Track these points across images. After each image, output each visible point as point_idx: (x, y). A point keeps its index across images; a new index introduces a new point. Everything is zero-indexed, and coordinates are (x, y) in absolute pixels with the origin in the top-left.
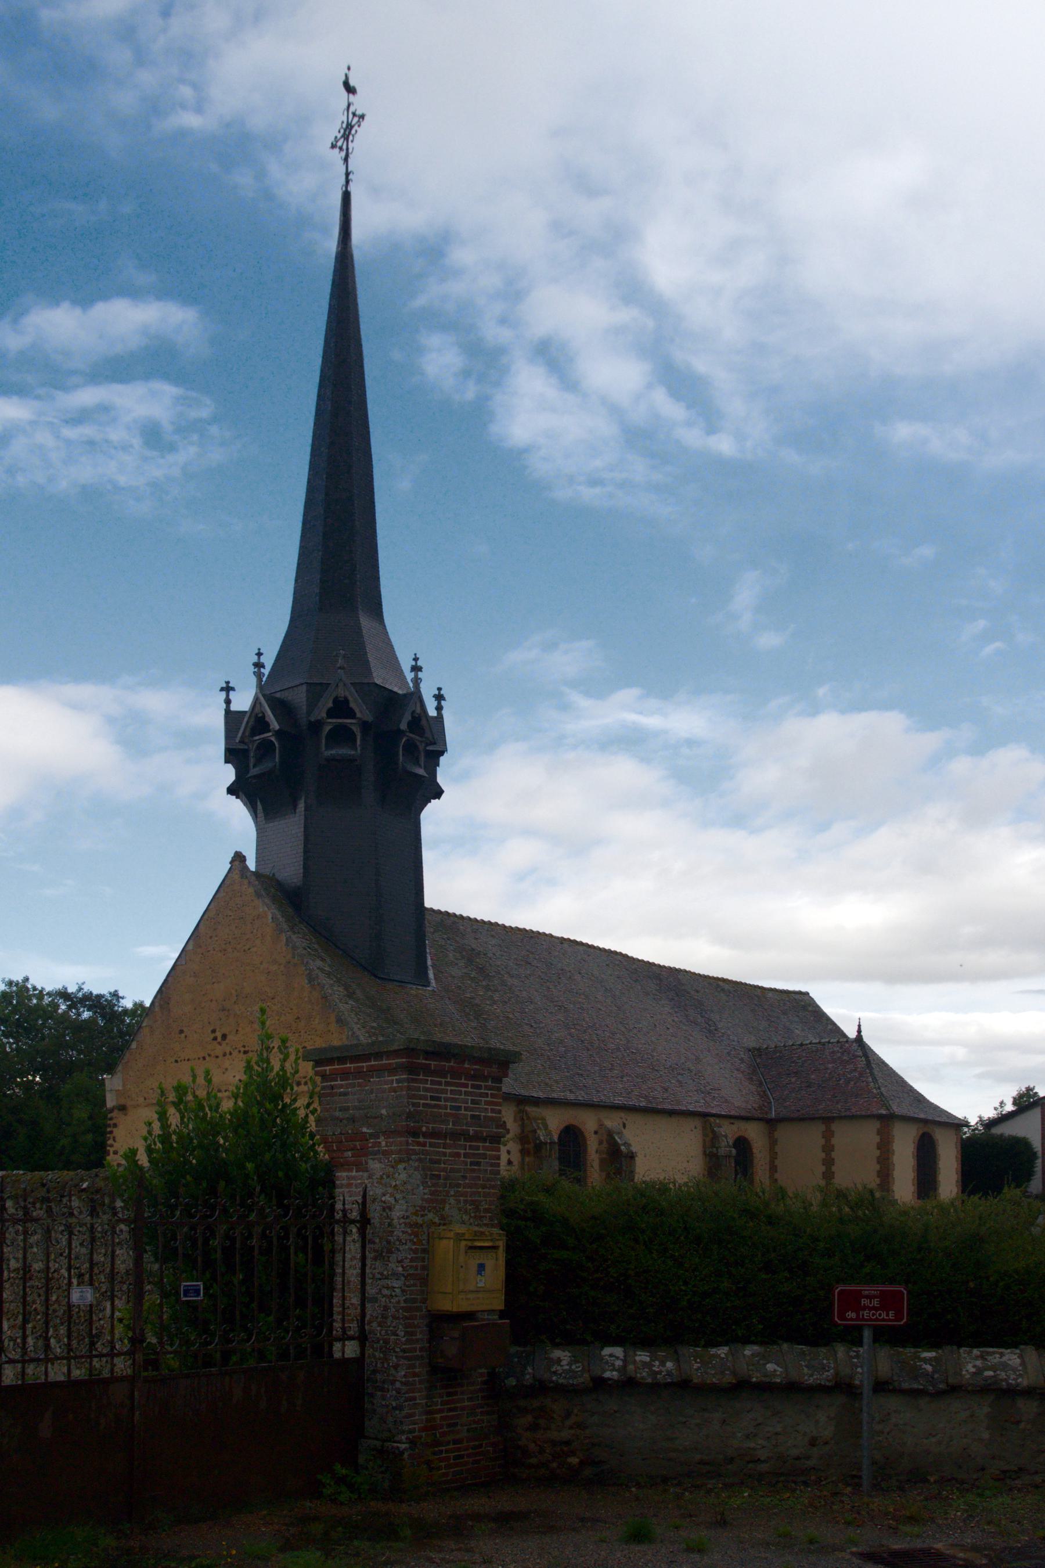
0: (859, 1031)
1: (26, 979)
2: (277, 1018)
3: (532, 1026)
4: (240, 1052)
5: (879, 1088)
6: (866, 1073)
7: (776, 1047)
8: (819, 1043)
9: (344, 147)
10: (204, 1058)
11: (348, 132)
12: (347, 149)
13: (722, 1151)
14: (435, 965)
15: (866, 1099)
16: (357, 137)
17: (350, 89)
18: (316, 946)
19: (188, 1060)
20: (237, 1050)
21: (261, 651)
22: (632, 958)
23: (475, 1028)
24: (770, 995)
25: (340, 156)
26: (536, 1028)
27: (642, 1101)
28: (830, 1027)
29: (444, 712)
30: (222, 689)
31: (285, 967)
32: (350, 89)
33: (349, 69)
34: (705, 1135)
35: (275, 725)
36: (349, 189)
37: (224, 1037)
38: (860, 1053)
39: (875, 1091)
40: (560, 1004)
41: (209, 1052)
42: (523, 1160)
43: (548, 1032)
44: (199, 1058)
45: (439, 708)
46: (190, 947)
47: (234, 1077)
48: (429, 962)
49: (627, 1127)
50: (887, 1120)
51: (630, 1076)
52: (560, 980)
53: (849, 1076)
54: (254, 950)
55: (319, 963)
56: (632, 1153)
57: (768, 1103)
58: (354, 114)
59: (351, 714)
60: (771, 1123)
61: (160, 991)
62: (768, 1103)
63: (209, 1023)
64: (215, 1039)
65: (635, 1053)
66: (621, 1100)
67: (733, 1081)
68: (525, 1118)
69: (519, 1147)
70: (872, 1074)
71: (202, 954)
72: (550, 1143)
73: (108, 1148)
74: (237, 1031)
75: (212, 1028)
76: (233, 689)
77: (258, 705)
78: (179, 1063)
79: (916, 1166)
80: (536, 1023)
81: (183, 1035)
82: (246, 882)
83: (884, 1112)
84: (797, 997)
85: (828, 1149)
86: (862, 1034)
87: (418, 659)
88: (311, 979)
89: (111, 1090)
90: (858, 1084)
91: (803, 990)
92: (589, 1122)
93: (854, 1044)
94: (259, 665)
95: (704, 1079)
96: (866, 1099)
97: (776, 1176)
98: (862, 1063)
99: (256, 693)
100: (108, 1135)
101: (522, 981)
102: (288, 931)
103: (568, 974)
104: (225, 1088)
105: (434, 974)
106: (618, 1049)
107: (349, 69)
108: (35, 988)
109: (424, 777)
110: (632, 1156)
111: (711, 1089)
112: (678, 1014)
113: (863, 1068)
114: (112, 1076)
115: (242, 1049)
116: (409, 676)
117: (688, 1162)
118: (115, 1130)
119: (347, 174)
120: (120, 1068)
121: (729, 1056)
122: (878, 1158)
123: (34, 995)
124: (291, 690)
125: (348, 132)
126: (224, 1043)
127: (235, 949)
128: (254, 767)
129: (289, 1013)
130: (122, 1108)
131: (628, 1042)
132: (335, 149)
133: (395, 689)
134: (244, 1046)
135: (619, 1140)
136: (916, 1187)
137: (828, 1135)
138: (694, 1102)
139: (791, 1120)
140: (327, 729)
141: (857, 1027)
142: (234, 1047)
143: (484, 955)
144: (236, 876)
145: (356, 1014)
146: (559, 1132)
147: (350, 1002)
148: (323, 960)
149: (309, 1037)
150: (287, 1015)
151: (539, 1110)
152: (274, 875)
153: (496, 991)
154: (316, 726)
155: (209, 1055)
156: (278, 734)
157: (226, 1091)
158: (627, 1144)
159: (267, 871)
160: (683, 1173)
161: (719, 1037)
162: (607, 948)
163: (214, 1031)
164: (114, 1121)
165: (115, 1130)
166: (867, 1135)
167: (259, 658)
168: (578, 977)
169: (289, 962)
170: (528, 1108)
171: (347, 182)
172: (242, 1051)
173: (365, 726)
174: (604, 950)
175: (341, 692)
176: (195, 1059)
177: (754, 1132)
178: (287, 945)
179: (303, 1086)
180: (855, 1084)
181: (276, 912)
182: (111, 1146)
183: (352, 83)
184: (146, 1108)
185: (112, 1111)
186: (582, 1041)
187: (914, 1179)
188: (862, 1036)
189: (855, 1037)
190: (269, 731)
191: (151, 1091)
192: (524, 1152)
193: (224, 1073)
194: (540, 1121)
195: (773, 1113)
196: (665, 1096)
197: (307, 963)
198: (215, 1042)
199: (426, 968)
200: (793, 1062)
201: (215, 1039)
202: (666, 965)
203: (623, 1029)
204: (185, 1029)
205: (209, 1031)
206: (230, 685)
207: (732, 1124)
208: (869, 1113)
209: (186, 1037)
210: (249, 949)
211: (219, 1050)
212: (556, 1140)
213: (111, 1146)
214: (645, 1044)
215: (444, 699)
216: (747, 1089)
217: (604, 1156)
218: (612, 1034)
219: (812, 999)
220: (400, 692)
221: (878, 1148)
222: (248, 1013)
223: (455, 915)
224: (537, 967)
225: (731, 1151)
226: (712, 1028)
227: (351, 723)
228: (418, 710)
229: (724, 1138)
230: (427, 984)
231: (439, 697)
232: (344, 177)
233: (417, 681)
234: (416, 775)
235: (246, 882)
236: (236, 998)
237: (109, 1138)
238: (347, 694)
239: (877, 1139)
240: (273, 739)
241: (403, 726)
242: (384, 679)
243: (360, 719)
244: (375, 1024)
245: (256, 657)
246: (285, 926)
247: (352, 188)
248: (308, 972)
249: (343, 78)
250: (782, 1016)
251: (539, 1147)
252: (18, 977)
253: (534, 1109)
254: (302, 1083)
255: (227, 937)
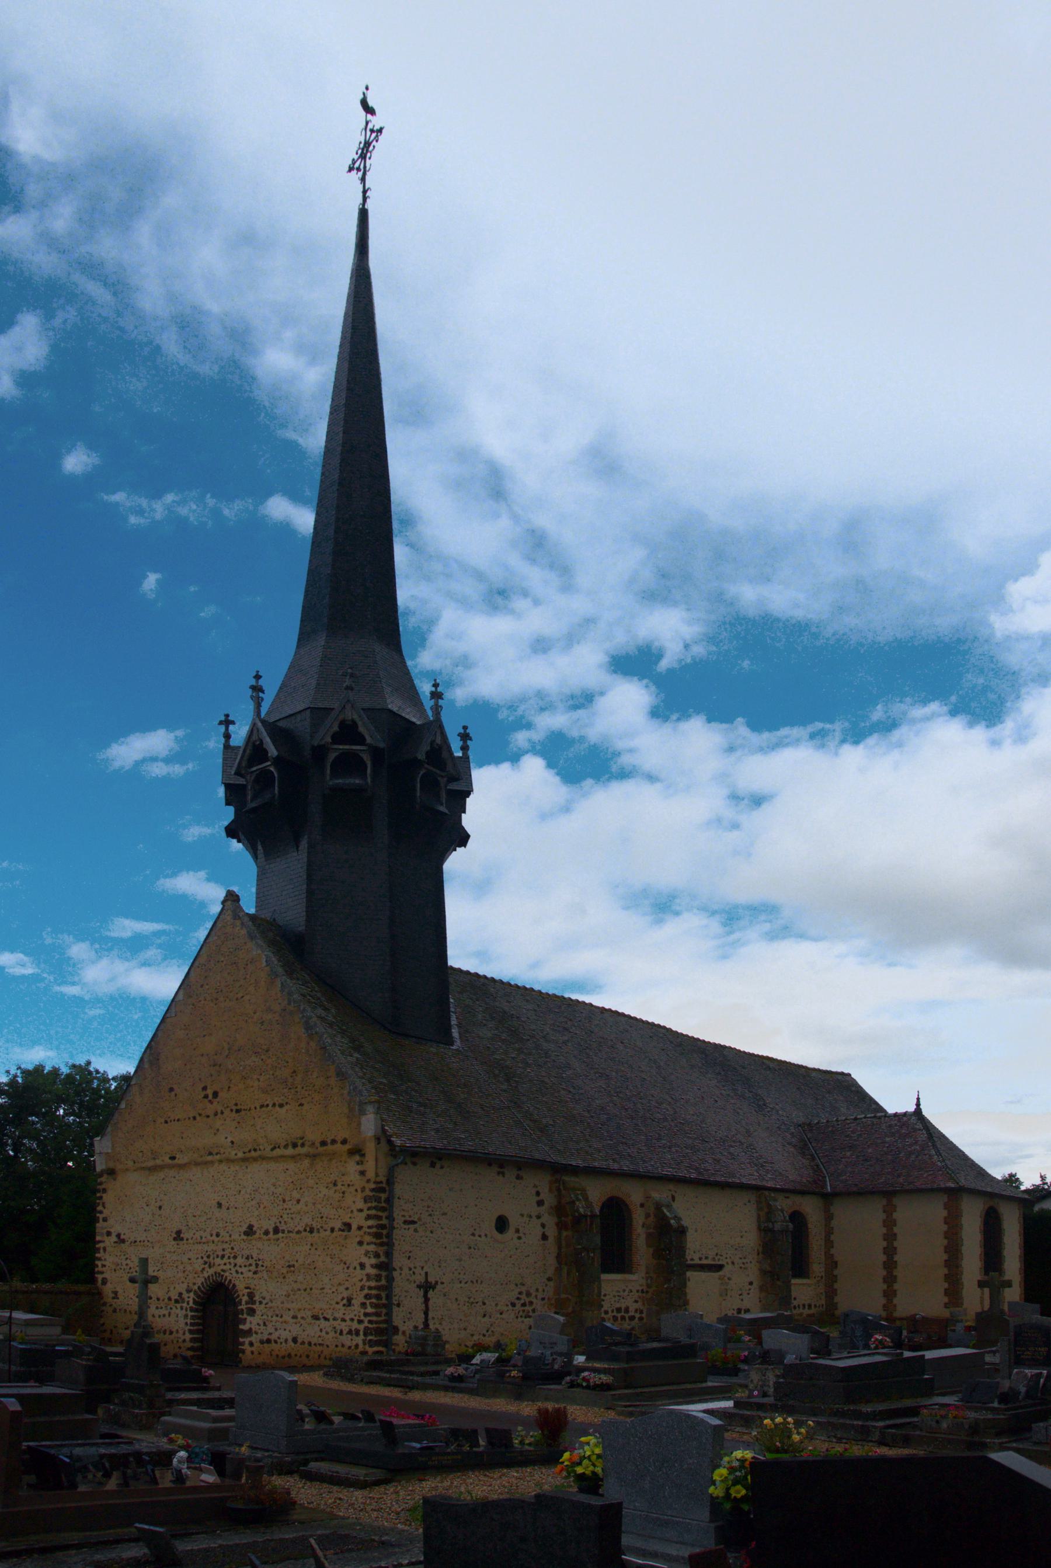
0: (918, 1104)
1: (89, 1063)
2: (271, 1073)
3: (570, 1092)
4: (232, 1110)
5: (944, 1161)
6: (928, 1146)
7: (828, 1121)
8: (875, 1117)
9: (362, 167)
10: (194, 1118)
11: (365, 150)
12: (365, 167)
13: (778, 1226)
14: (460, 1024)
15: (932, 1172)
16: (374, 152)
17: (369, 110)
18: (319, 995)
19: (178, 1120)
20: (229, 1109)
21: (260, 674)
22: (676, 1032)
23: (505, 1091)
24: (814, 1074)
25: (357, 177)
26: (575, 1094)
27: (693, 1173)
28: (874, 1106)
29: (470, 753)
30: (221, 723)
31: (280, 1015)
32: (369, 110)
33: (367, 88)
34: (759, 1209)
35: (273, 751)
36: (366, 207)
37: (215, 1094)
38: (920, 1126)
39: (939, 1164)
40: (601, 1071)
41: (200, 1112)
42: (560, 1233)
43: (588, 1098)
44: (189, 1118)
45: (465, 748)
46: (181, 997)
47: (226, 1138)
48: (454, 1021)
49: (677, 1199)
50: (954, 1194)
51: (678, 1146)
52: (601, 1048)
53: (909, 1149)
54: (247, 998)
55: (320, 1011)
56: (683, 1227)
57: (823, 1177)
58: (372, 131)
59: (360, 740)
60: (828, 1198)
61: (149, 1046)
62: (823, 1177)
63: (200, 1079)
64: (206, 1097)
65: (683, 1124)
66: (670, 1171)
67: (786, 1155)
68: (561, 1187)
69: (556, 1220)
70: (934, 1146)
71: (193, 1005)
72: (590, 1216)
73: (98, 1215)
74: (229, 1087)
75: (203, 1085)
76: (233, 723)
77: (255, 732)
78: (169, 1124)
79: (983, 1241)
80: (574, 1088)
81: (173, 1093)
82: (238, 923)
83: (953, 1186)
84: (840, 1077)
85: (889, 1223)
86: (921, 1107)
87: (438, 685)
88: (308, 1027)
89: (100, 1153)
90: (920, 1157)
91: (846, 1071)
92: (634, 1194)
93: (913, 1118)
94: (257, 689)
95: (756, 1152)
96: (932, 1172)
97: (832, 1251)
98: (923, 1136)
99: (253, 719)
100: (98, 1201)
101: (560, 1047)
102: (283, 975)
103: (610, 1042)
104: (216, 1151)
105: (460, 1033)
106: (665, 1120)
107: (367, 88)
108: (97, 1072)
109: (446, 814)
110: (682, 1231)
111: (765, 1162)
112: (726, 1088)
113: (924, 1141)
114: (102, 1137)
115: (234, 1108)
116: (428, 704)
117: (742, 1237)
118: (104, 1195)
119: (365, 192)
120: (109, 1129)
121: (780, 1130)
122: (946, 1233)
123: (96, 1078)
124: (293, 717)
125: (365, 150)
126: (215, 1101)
127: (227, 997)
128: (252, 801)
129: (285, 1066)
130: (111, 1172)
131: (675, 1112)
132: (352, 172)
133: (414, 720)
134: (236, 1105)
135: (668, 1214)
136: (983, 1263)
137: (889, 1210)
138: (749, 1175)
139: (849, 1194)
140: (332, 756)
141: (915, 1101)
142: (225, 1105)
143: (518, 1018)
144: (228, 917)
145: (361, 1068)
146: (600, 1204)
147: (356, 1055)
148: (326, 1009)
149: (307, 1093)
150: (283, 1069)
151: (577, 1180)
152: (274, 920)
153: (530, 1054)
154: (319, 752)
155: (200, 1115)
156: (277, 761)
157: (217, 1154)
158: (678, 1219)
159: (266, 915)
160: (736, 1249)
161: (768, 1112)
162: (650, 1021)
163: (205, 1088)
164: (103, 1186)
165: (104, 1195)
166: (934, 1211)
167: (257, 682)
168: (621, 1047)
169: (285, 1010)
170: (566, 1178)
171: (365, 199)
172: (234, 1111)
173: (377, 753)
174: (647, 1022)
175: (350, 715)
176: (185, 1119)
177: (811, 1208)
178: (282, 991)
179: (299, 1148)
180: (917, 1157)
181: (270, 954)
182: (101, 1212)
183: (371, 103)
184: (135, 1172)
185: (101, 1175)
186: (626, 1109)
187: (981, 1255)
188: (921, 1109)
189: (913, 1110)
190: (267, 760)
191: (141, 1154)
192: (561, 1226)
193: (215, 1134)
194: (579, 1192)
195: (829, 1188)
196: (718, 1167)
197: (304, 1009)
198: (206, 1100)
199: (450, 1027)
200: (847, 1136)
201: (206, 1097)
202: (711, 1042)
203: (670, 1100)
204: (175, 1087)
205: (200, 1089)
206: (230, 718)
207: (788, 1197)
208: (935, 1186)
209: (176, 1095)
210: (243, 997)
211: (210, 1109)
212: (598, 1213)
213: (101, 1212)
214: (693, 1115)
215: (471, 739)
216: (800, 1163)
217: (651, 1230)
218: (658, 1103)
219: (855, 1080)
220: (418, 723)
221: (946, 1223)
222: (241, 1068)
223: (485, 977)
224: (576, 1034)
225: (787, 1226)
226: (761, 1103)
227: (361, 750)
228: (439, 740)
229: (780, 1212)
230: (450, 1042)
231: (465, 737)
232: (361, 195)
233: (437, 709)
234: (438, 812)
235: (238, 923)
236: (227, 1052)
237: (99, 1204)
238: (355, 717)
239: (945, 1213)
240: (272, 769)
241: (421, 756)
242: (400, 707)
243: (369, 746)
244: (384, 1081)
245: (254, 680)
246: (280, 970)
247: (369, 205)
248: (305, 1019)
249: (362, 96)
250: (827, 1095)
251: (578, 1220)
252: (81, 1061)
253: (573, 1179)
254: (299, 1144)
255: (219, 984)
